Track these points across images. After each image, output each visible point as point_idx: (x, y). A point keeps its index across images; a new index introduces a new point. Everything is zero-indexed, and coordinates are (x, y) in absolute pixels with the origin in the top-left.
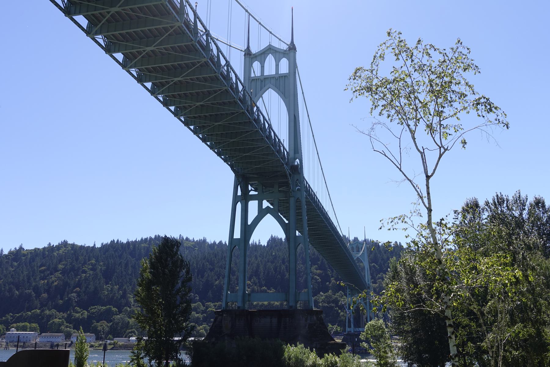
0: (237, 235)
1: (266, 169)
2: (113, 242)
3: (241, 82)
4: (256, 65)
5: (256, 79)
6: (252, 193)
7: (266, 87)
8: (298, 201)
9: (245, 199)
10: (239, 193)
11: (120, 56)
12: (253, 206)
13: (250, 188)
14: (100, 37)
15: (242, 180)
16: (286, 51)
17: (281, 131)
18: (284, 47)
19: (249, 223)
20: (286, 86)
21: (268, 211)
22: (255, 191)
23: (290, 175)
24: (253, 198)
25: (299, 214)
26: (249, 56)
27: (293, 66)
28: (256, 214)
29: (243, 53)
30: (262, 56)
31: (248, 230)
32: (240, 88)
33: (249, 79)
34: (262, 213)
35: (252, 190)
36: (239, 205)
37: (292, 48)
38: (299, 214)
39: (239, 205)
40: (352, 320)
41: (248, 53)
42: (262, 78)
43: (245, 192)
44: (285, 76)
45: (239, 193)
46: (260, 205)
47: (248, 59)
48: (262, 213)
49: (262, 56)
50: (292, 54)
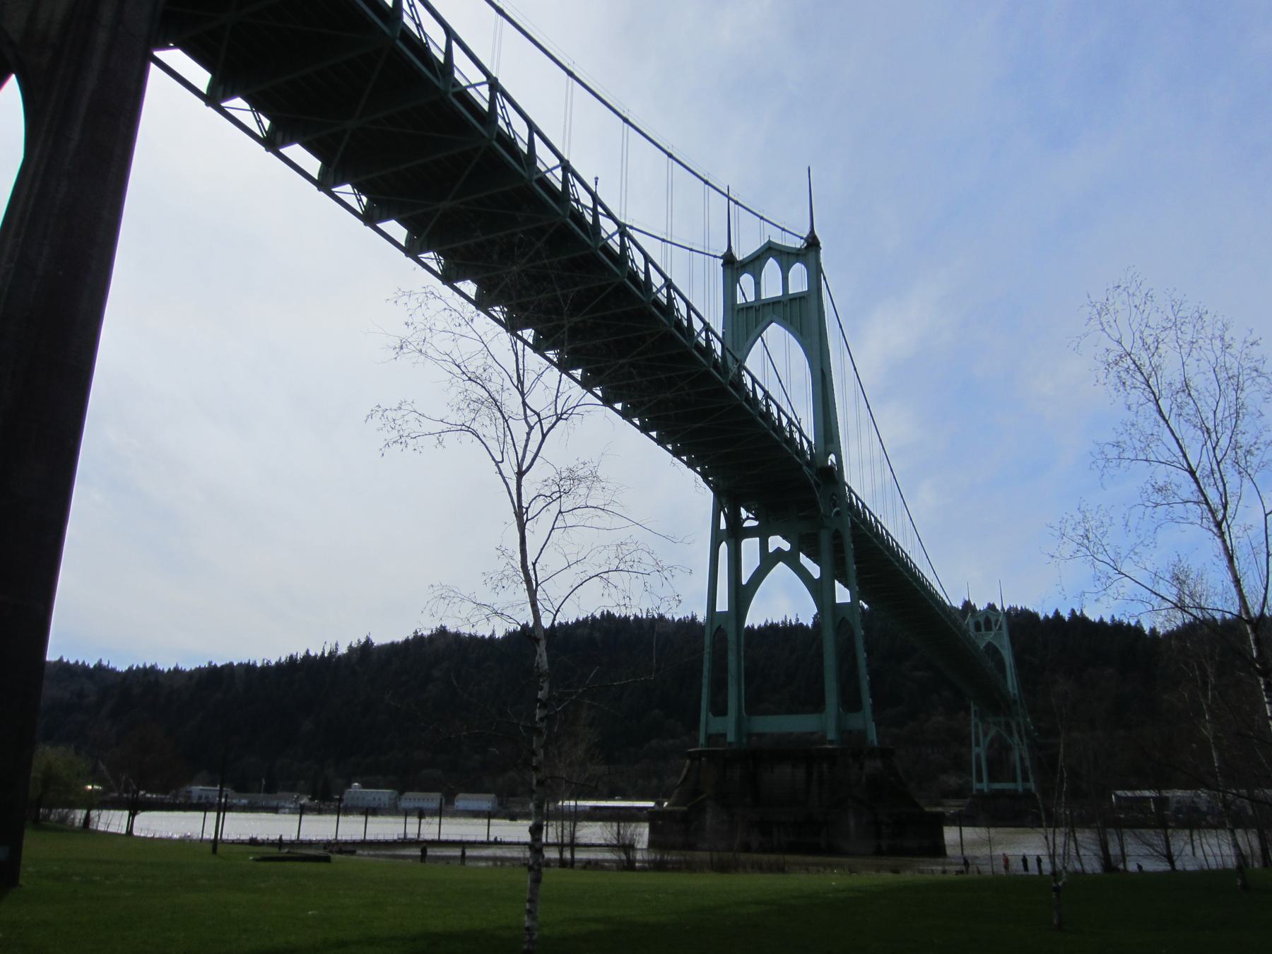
0: (722, 605)
1: (770, 478)
2: (130, 669)
3: (716, 336)
4: (746, 280)
5: (748, 308)
6: (747, 524)
7: (768, 319)
8: (837, 536)
9: (735, 534)
10: (723, 525)
11: (470, 287)
12: (750, 547)
13: (744, 513)
14: (431, 254)
15: (728, 498)
16: (799, 250)
17: (795, 407)
18: (798, 244)
19: (744, 582)
20: (803, 315)
21: (779, 555)
22: (755, 519)
23: (818, 485)
24: (750, 532)
25: (838, 549)
26: (732, 266)
27: (816, 273)
28: (757, 563)
29: (721, 261)
30: (754, 264)
31: (742, 595)
32: (717, 346)
33: (733, 309)
34: (768, 560)
35: (748, 518)
36: (724, 548)
37: (813, 243)
38: (838, 549)
39: (724, 548)
40: (1028, 763)
41: (729, 260)
42: (756, 304)
43: (735, 521)
44: (800, 298)
45: (723, 525)
46: (764, 546)
47: (729, 271)
48: (768, 560)
49: (754, 264)
50: (811, 255)
